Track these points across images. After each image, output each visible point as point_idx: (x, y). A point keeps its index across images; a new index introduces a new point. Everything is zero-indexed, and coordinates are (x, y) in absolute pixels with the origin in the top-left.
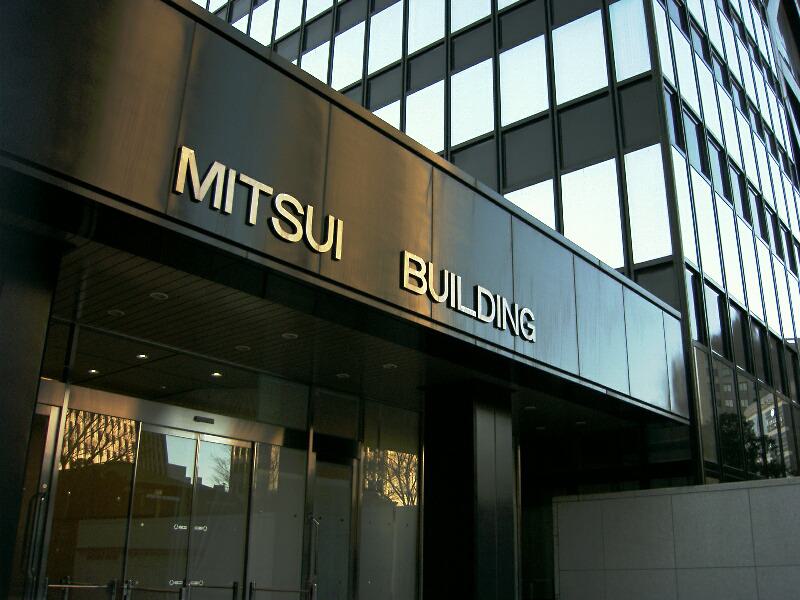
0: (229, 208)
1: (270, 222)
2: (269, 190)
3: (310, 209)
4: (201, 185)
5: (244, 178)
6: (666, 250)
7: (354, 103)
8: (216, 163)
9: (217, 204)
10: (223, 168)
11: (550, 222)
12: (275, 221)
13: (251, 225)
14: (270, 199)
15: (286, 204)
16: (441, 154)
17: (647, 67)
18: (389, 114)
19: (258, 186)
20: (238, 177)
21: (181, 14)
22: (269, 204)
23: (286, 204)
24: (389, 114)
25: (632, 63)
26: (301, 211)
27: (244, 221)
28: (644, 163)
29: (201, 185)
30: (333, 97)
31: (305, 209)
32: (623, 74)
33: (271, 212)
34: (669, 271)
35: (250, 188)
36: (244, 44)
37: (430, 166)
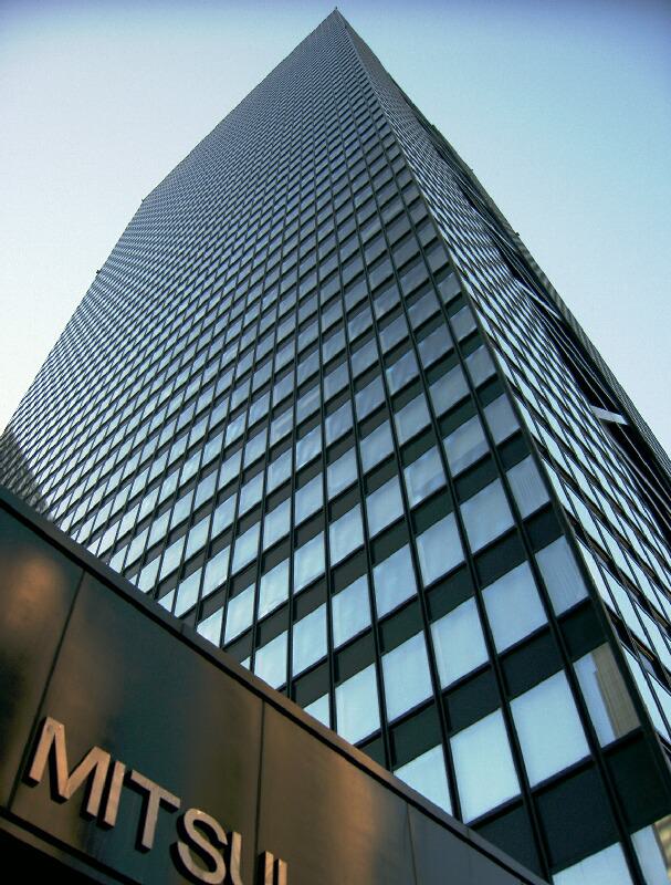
0: (111, 816)
1: (174, 850)
2: (175, 801)
3: (237, 839)
4: (70, 775)
5: (137, 777)
6: (581, 594)
7: (284, 701)
8: (96, 748)
9: (93, 808)
10: (107, 758)
11: (447, 808)
12: (183, 849)
13: (144, 850)
14: (176, 816)
15: (198, 824)
16: (281, 689)
17: (635, 723)
18: (318, 711)
19: (157, 793)
20: (128, 776)
21: (374, 781)
22: (174, 824)
23: (198, 824)
24: (318, 711)
25: (567, 596)
26: (223, 839)
27: (132, 839)
28: (586, 668)
29: (70, 775)
30: (270, 696)
31: (230, 837)
32: (560, 608)
33: (176, 836)
34: (427, 220)
35: (146, 794)
36: (200, 648)
37: (260, 700)
